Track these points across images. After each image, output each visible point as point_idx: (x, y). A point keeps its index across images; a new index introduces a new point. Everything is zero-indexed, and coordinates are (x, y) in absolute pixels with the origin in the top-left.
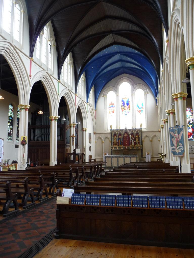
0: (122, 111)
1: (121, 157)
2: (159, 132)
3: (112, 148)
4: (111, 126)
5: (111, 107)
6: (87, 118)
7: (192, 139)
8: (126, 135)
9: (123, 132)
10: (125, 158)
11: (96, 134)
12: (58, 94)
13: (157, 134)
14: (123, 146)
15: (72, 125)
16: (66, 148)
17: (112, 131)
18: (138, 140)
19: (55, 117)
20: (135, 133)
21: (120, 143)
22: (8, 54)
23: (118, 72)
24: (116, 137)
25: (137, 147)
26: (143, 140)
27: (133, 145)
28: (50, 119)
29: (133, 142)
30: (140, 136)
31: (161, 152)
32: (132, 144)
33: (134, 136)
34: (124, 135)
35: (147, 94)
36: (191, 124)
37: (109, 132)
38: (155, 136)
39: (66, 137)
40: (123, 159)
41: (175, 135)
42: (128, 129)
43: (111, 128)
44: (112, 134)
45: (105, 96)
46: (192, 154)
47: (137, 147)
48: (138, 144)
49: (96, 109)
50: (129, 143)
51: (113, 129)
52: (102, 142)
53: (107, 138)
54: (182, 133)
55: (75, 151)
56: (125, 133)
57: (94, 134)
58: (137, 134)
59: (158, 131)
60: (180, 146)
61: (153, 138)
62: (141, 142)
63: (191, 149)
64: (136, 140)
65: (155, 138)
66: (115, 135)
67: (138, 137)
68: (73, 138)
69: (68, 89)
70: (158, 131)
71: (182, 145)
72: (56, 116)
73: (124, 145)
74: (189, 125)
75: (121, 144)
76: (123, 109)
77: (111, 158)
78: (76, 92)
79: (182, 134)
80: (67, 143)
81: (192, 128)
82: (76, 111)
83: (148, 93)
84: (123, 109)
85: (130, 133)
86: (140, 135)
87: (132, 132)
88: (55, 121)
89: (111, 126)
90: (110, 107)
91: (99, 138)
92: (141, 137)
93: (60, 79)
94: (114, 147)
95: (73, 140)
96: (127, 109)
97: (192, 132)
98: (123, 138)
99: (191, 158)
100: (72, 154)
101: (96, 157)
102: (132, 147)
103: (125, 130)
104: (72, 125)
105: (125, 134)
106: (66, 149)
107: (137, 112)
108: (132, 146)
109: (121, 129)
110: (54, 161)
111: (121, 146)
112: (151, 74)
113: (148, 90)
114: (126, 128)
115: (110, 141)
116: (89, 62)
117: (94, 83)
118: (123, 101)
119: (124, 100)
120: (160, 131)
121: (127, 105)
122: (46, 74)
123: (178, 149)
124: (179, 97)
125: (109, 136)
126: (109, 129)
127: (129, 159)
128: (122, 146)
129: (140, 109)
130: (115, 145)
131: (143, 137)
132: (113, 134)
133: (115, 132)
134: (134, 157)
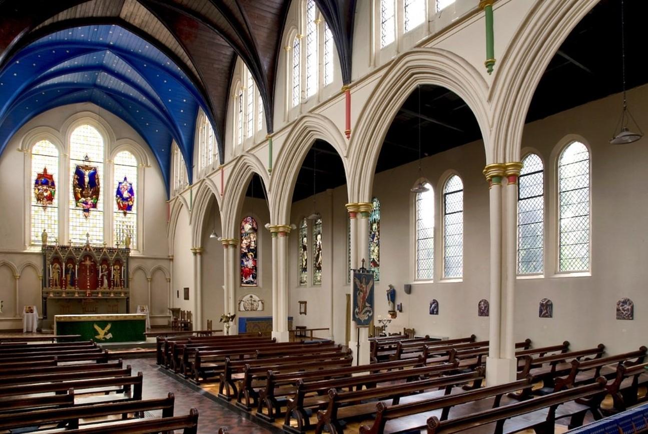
0: (77, 199)
2: (169, 261)
3: (48, 293)
4: (44, 236)
7: (252, 282)
9: (81, 254)
13: (164, 264)
14: (77, 289)
17: (46, 249)
18: (121, 276)
20: (112, 258)
21: (69, 282)
22: (395, 98)
23: (75, 94)
25: (117, 293)
26: (130, 276)
27: (105, 289)
29: (106, 281)
31: (170, 305)
32: (102, 285)
34: (84, 261)
35: (147, 169)
36: (252, 251)
37: (38, 250)
38: (159, 269)
41: (361, 287)
42: (95, 249)
44: (47, 258)
45: (27, 150)
46: (251, 310)
47: (117, 293)
51: (51, 242)
53: (30, 265)
54: (372, 284)
56: (93, 262)
58: (118, 262)
59: (166, 257)
60: (366, 309)
61: (153, 273)
62: (125, 282)
63: (250, 302)
65: (159, 275)
66: (56, 260)
70: (167, 259)
71: (370, 307)
73: (83, 286)
74: (249, 252)
75: (73, 284)
76: (79, 195)
79: (370, 286)
81: (253, 260)
84: (79, 195)
85: (98, 258)
87: (103, 257)
97: (253, 267)
99: (126, 312)
103: (86, 250)
105: (91, 262)
108: (102, 290)
111: (73, 289)
113: (149, 157)
115: (41, 274)
117: (11, 109)
119: (83, 171)
120: (171, 258)
121: (91, 187)
123: (364, 314)
124: (362, 212)
125: (38, 262)
131: (131, 270)
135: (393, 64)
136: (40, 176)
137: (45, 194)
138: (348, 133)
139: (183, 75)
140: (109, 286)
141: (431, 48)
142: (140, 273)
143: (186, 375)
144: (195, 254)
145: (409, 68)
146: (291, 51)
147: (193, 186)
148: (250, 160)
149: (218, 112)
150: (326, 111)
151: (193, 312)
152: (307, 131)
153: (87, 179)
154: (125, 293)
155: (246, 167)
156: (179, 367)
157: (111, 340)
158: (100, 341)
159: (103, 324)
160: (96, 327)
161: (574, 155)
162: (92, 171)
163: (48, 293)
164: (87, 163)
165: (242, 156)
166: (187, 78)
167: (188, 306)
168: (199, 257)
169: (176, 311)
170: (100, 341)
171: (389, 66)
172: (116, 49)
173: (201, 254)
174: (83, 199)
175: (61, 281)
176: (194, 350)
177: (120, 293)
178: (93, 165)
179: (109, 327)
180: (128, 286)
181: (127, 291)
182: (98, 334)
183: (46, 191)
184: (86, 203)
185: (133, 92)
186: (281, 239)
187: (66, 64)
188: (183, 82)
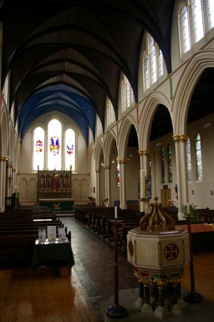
0: (51, 150)
20: (65, 175)
38: (84, 179)
43: (38, 169)
50: (58, 186)
51: (41, 169)
52: (27, 184)
53: (33, 179)
58: (67, 176)
61: (82, 181)
62: (70, 186)
66: (43, 176)
68: (10, 180)
73: (52, 187)
75: (49, 187)
94: (47, 190)
102: (61, 190)
118: (52, 140)
125: (36, 178)
135: (189, 61)
138: (171, 98)
140: (63, 187)
141: (208, 48)
142: (76, 181)
143: (110, 239)
144: (97, 172)
145: (198, 61)
146: (123, 88)
147: (172, 74)
148: (129, 117)
149: (114, 96)
150: (160, 89)
151: (96, 198)
152: (154, 100)
153: (55, 142)
155: (128, 121)
156: (112, 237)
157: (60, 210)
158: (55, 210)
159: (57, 203)
160: (55, 204)
162: (57, 139)
163: (39, 190)
165: (125, 116)
167: (95, 195)
168: (98, 173)
169: (91, 198)
170: (55, 210)
171: (187, 63)
172: (70, 74)
175: (44, 185)
176: (107, 220)
177: (67, 190)
179: (59, 204)
180: (71, 187)
181: (39, 189)
182: (55, 207)
184: (54, 152)
185: (71, 106)
186: (145, 157)
187: (46, 99)
188: (87, 101)
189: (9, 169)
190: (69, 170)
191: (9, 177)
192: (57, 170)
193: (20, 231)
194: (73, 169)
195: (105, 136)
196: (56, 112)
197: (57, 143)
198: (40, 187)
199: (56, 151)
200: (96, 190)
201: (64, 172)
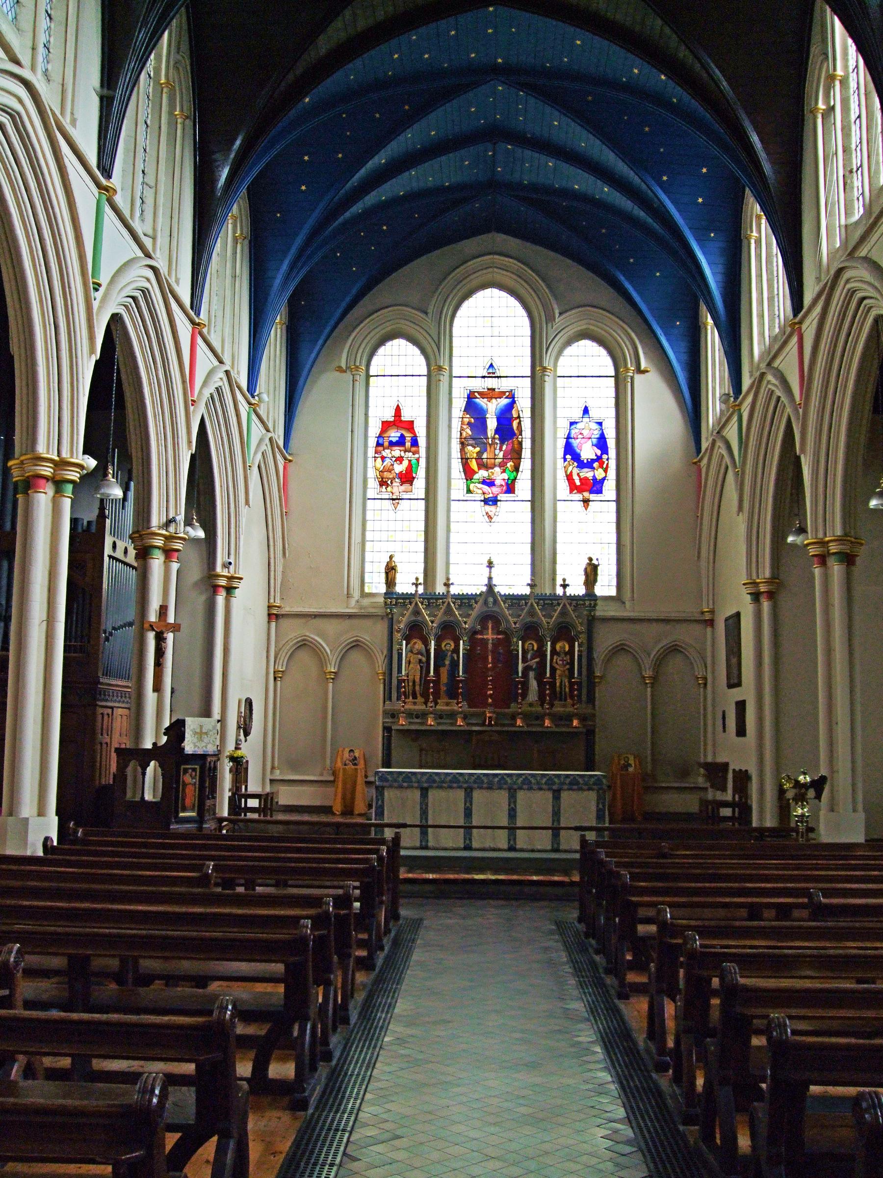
0: (469, 473)
1: (490, 785)
4: (390, 570)
5: (392, 444)
6: (247, 502)
8: (490, 636)
9: (474, 614)
10: (431, 794)
11: (283, 615)
12: (97, 286)
15: (159, 542)
16: (100, 710)
18: (571, 670)
19: (61, 464)
20: (547, 622)
24: (450, 645)
27: (531, 705)
28: (16, 475)
30: (579, 646)
32: (524, 695)
33: (542, 645)
38: (674, 649)
39: (103, 627)
40: (502, 797)
43: (390, 582)
48: (562, 698)
49: (293, 443)
52: (324, 677)
55: (177, 730)
57: (269, 615)
58: (563, 632)
61: (659, 663)
64: (553, 670)
65: (675, 664)
66: (415, 630)
67: (571, 652)
68: (160, 639)
69: (153, 268)
70: (697, 621)
72: (65, 454)
73: (475, 698)
75: (452, 694)
76: (474, 465)
77: (417, 794)
78: (196, 304)
80: (106, 674)
82: (190, 442)
83: (646, 371)
84: (474, 465)
86: (583, 638)
87: (528, 619)
88: (59, 491)
89: (390, 570)
90: (386, 444)
91: (304, 644)
92: (585, 654)
93: (110, 177)
94: (439, 716)
95: (160, 653)
96: (502, 465)
98: (468, 656)
100: (156, 752)
101: (277, 775)
102: (526, 716)
104: (159, 542)
106: (100, 717)
107: (563, 486)
108: (526, 708)
109: (454, 590)
110: (35, 811)
112: (698, 240)
114: (490, 587)
116: (300, 106)
117: (310, 257)
118: (471, 406)
119: (481, 402)
120: (707, 617)
122: (20, 101)
126: (376, 584)
127: (545, 798)
128: (460, 706)
129: (588, 474)
130: (415, 697)
132: (402, 626)
133: (417, 612)
134: (580, 789)
136: (386, 426)
137: (399, 468)
139: (677, 94)
144: (756, 597)
153: (492, 424)
154: (583, 719)
161: (490, 565)
162: (504, 402)
163: (393, 715)
164: (491, 383)
166: (686, 98)
168: (766, 605)
173: (771, 595)
174: (483, 474)
175: (425, 682)
177: (569, 718)
178: (504, 385)
180: (591, 699)
183: (400, 459)
184: (490, 483)
187: (381, 159)
189: (157, 562)
190: (577, 589)
191: (153, 617)
192: (502, 589)
193: (696, 899)
194: (606, 586)
195: (809, 328)
196: (500, 239)
197: (506, 418)
198: (437, 696)
199: (499, 476)
200: (719, 723)
201: (550, 602)
